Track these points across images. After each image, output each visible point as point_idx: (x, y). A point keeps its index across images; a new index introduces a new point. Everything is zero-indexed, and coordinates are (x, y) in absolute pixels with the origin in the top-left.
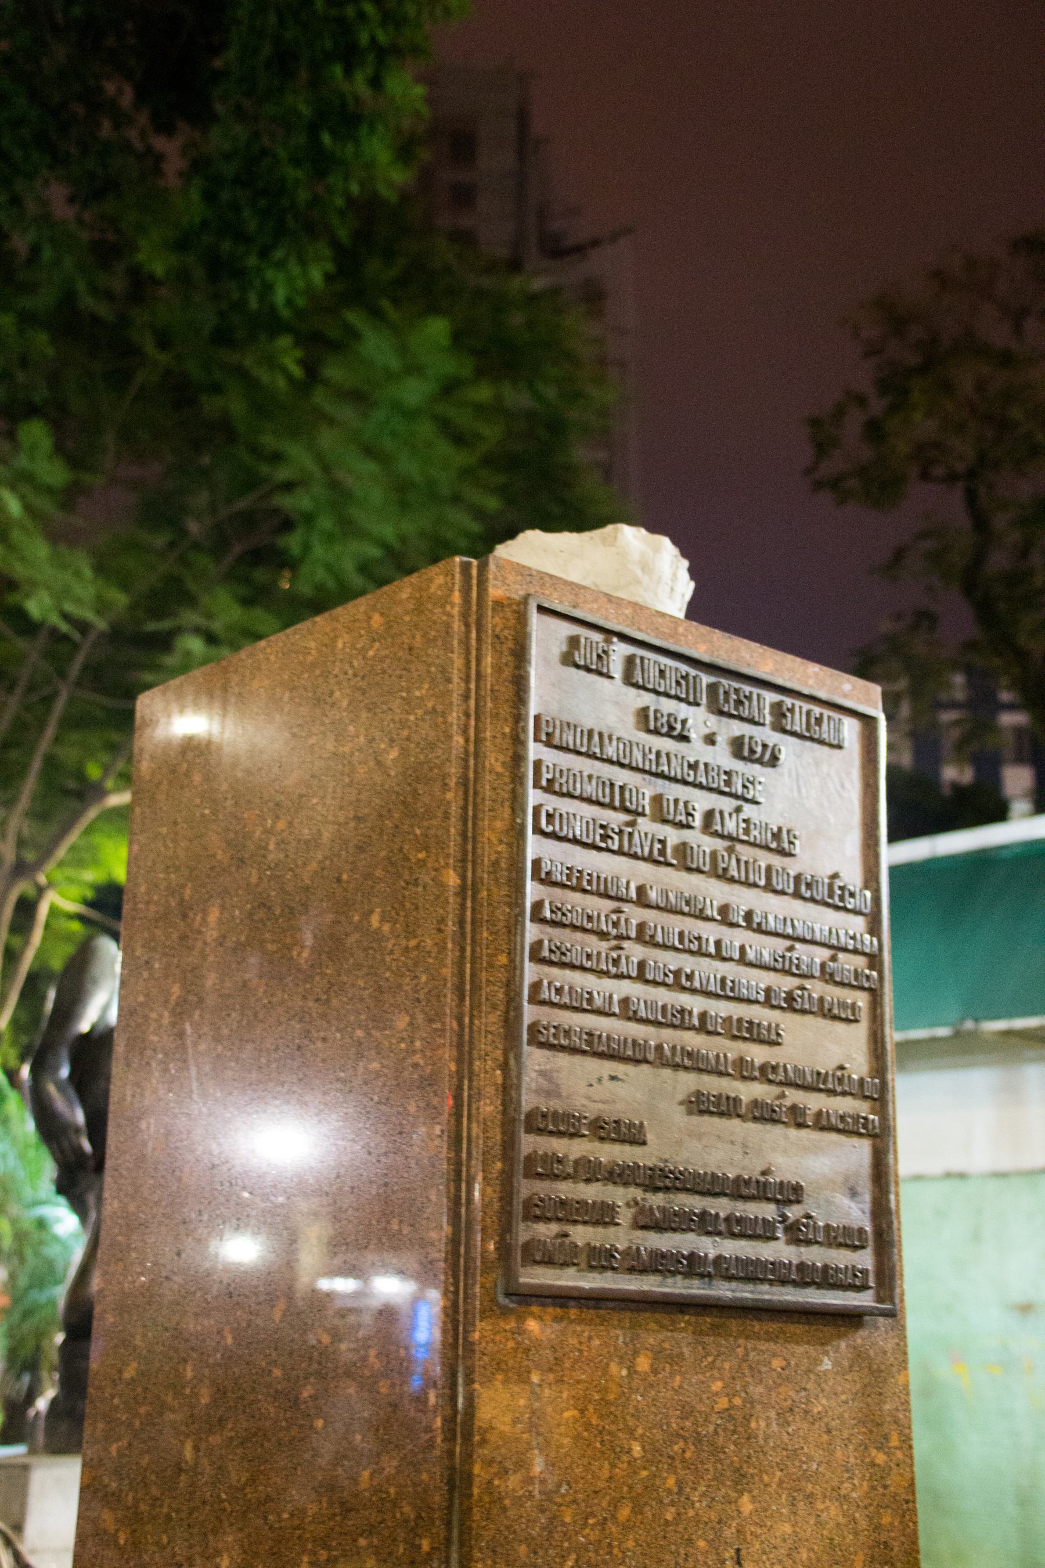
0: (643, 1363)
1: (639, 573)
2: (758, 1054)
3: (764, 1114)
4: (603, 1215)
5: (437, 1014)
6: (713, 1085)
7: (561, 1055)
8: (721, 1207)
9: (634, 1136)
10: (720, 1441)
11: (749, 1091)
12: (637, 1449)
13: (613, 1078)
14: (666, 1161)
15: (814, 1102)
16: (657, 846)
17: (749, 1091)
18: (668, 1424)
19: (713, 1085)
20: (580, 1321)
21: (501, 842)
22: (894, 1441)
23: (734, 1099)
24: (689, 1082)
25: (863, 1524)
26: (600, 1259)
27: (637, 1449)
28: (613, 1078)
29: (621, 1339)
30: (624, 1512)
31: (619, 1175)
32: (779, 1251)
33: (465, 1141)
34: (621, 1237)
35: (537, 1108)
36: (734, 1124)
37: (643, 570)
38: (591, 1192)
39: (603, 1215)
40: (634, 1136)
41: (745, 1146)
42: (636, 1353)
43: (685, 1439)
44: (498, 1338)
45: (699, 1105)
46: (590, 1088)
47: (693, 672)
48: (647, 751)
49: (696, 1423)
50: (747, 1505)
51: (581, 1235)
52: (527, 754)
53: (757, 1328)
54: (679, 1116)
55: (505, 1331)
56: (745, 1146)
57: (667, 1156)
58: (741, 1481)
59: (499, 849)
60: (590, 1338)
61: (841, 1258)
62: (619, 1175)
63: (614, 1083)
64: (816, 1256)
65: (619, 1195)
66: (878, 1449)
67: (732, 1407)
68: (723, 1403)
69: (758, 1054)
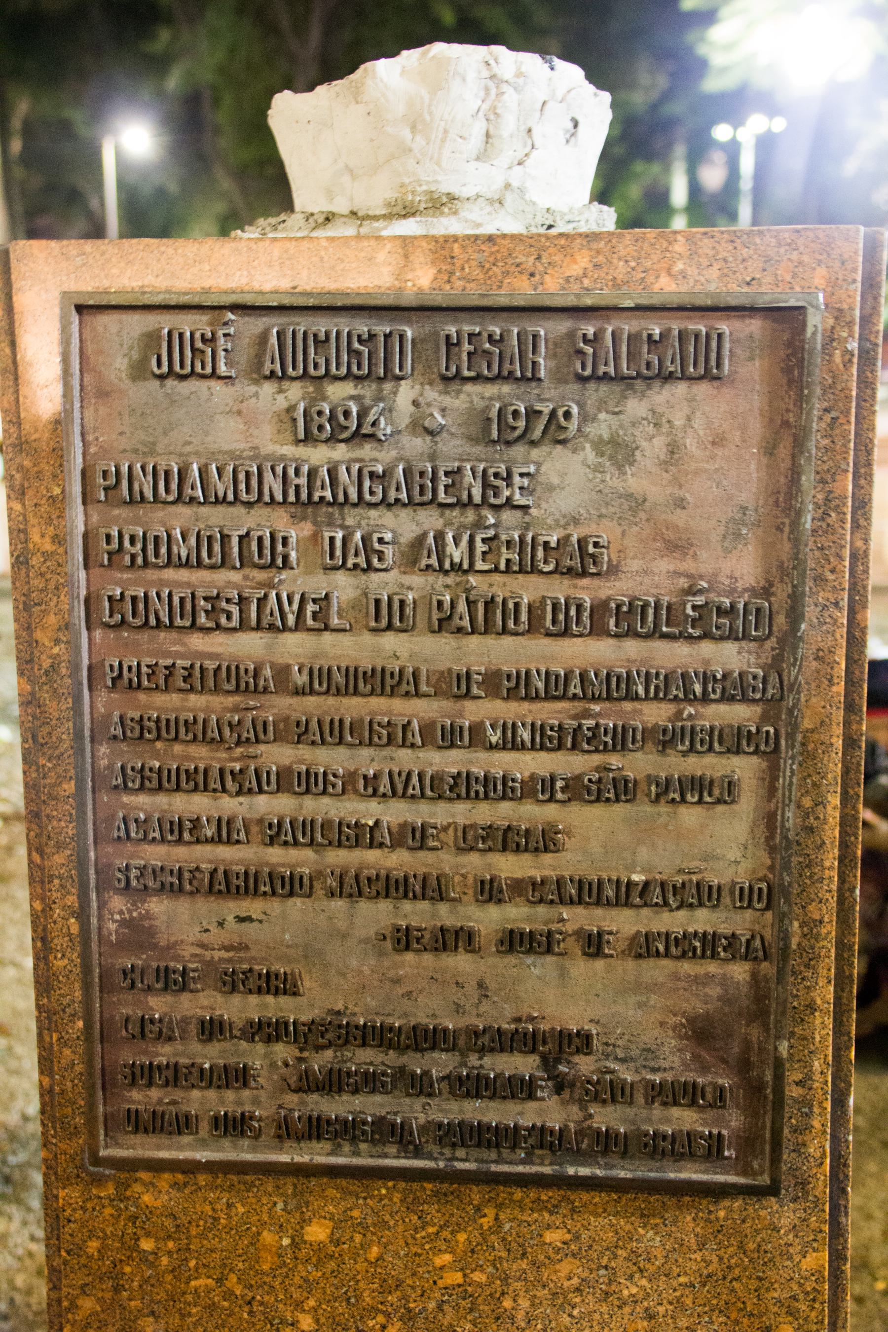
1: (407, 133)
3: (515, 942)
13: (241, 920)
14: (338, 1013)
18: (358, 1298)
19: (416, 913)
20: (213, 1188)
21: (57, 642)
28: (241, 920)
29: (280, 1206)
31: (268, 1031)
32: (550, 1112)
35: (657, 724)
37: (413, 128)
43: (388, 1315)
44: (89, 1205)
46: (205, 935)
47: (382, 329)
48: (291, 472)
49: (405, 1298)
55: (100, 1198)
57: (339, 1006)
59: (56, 650)
60: (229, 1206)
62: (268, 1031)
63: (245, 926)
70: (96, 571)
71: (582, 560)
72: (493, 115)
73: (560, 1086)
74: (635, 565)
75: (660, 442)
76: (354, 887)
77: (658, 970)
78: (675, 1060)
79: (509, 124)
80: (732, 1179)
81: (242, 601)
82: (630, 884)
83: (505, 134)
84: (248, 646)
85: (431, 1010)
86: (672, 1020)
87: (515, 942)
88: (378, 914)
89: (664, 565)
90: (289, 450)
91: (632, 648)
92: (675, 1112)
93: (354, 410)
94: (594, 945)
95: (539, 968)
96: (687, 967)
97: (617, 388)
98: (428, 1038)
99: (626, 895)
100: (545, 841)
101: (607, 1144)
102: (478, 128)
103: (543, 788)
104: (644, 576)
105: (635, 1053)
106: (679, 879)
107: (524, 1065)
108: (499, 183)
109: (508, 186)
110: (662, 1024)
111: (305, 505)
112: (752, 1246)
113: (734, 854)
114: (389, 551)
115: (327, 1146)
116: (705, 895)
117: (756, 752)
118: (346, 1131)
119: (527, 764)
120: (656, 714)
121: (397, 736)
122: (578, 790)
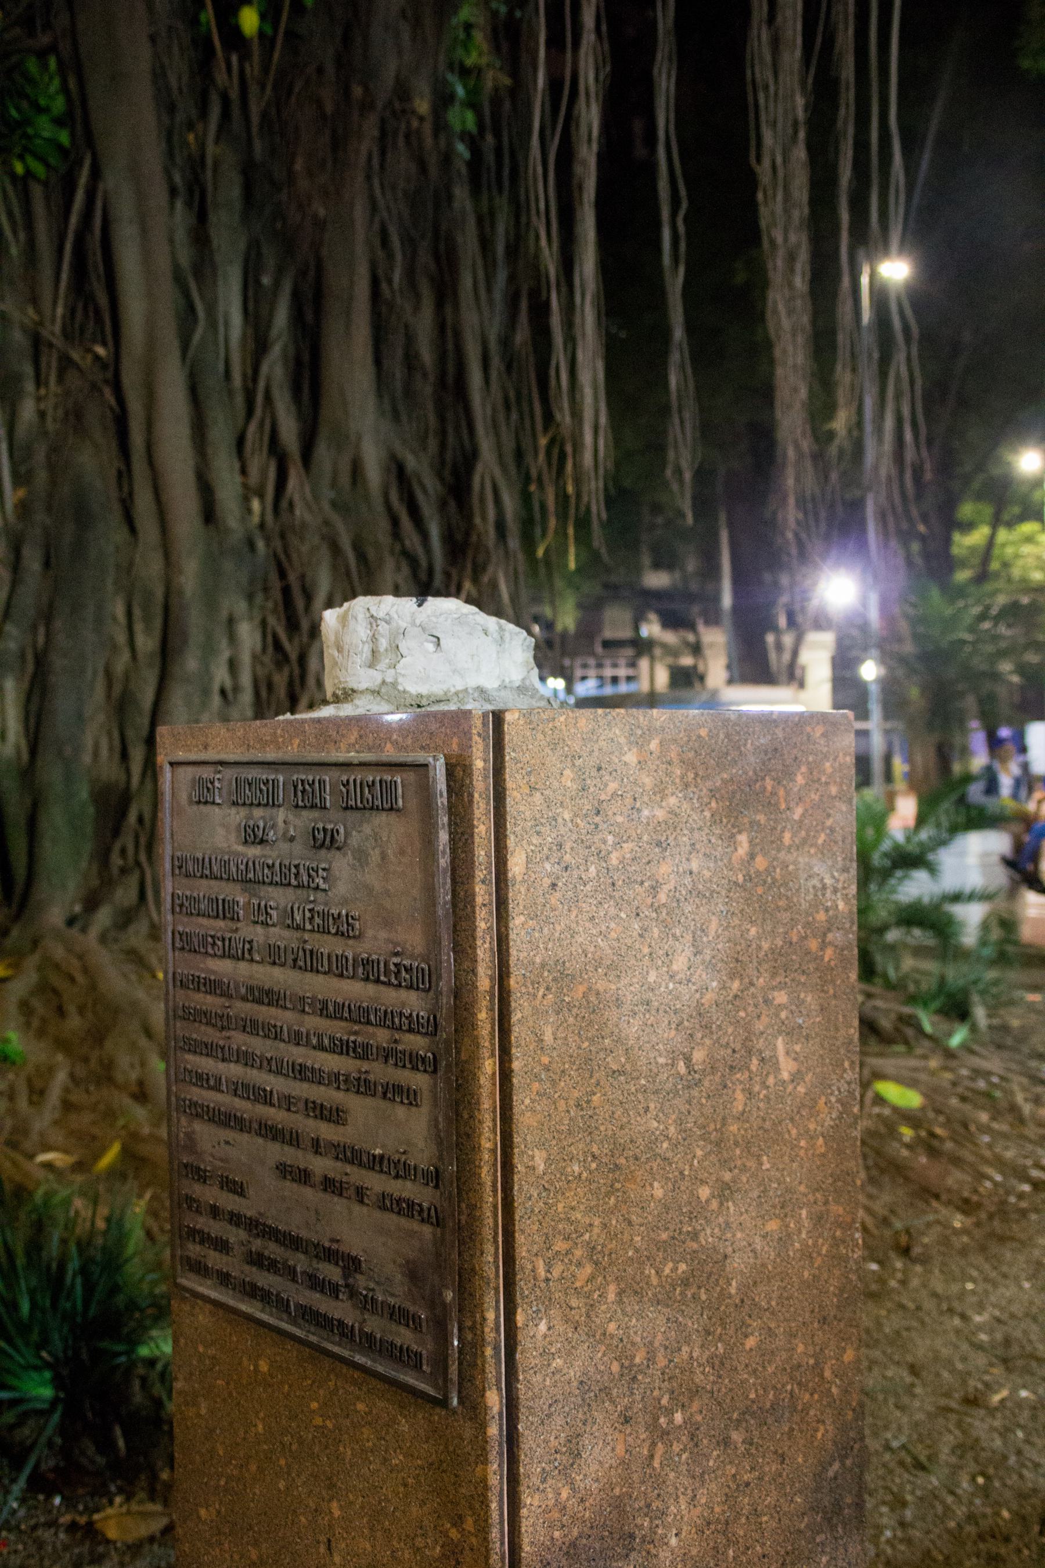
2: (326, 1131)
3: (330, 1185)
4: (222, 1246)
5: (838, 1246)
6: (291, 1155)
8: (300, 1262)
9: (237, 1189)
10: (316, 1449)
11: (321, 1165)
13: (227, 1143)
15: (376, 1183)
16: (247, 946)
17: (321, 1165)
22: (469, 1524)
23: (305, 1171)
28: (227, 1143)
34: (232, 1264)
36: (308, 1192)
38: (216, 1228)
39: (222, 1246)
40: (237, 1189)
41: (317, 1212)
42: (259, 1356)
45: (284, 1170)
52: (797, 714)
53: (344, 1371)
54: (270, 1180)
56: (317, 1212)
63: (227, 1147)
65: (235, 1235)
66: (454, 1525)
67: (324, 1427)
69: (326, 1131)
70: (177, 916)
71: (345, 928)
72: (374, 639)
73: (353, 1293)
74: (370, 933)
75: (377, 851)
76: (271, 1132)
77: (392, 1220)
78: (399, 1290)
79: (383, 644)
80: (422, 1386)
81: (223, 940)
82: (374, 1156)
83: (382, 649)
84: (222, 968)
85: (294, 1224)
86: (400, 1260)
87: (330, 1185)
88: (276, 1152)
89: (383, 935)
90: (240, 848)
91: (371, 989)
92: (402, 1330)
93: (261, 825)
94: (360, 1194)
95: (339, 1205)
96: (403, 1221)
97: (357, 815)
98: (294, 1243)
99: (376, 1163)
100: (334, 1115)
101: (369, 1343)
102: (367, 649)
103: (336, 1080)
104: (374, 942)
105: (383, 1279)
106: (396, 1157)
107: (332, 1272)
108: (379, 681)
109: (384, 682)
110: (394, 1262)
111: (248, 882)
112: (451, 1449)
113: (421, 1144)
114: (274, 913)
115: (259, 1305)
116: (402, 1170)
117: (425, 1071)
118: (263, 1296)
119: (331, 1062)
120: (381, 1036)
121: (274, 1033)
122: (363, 1086)
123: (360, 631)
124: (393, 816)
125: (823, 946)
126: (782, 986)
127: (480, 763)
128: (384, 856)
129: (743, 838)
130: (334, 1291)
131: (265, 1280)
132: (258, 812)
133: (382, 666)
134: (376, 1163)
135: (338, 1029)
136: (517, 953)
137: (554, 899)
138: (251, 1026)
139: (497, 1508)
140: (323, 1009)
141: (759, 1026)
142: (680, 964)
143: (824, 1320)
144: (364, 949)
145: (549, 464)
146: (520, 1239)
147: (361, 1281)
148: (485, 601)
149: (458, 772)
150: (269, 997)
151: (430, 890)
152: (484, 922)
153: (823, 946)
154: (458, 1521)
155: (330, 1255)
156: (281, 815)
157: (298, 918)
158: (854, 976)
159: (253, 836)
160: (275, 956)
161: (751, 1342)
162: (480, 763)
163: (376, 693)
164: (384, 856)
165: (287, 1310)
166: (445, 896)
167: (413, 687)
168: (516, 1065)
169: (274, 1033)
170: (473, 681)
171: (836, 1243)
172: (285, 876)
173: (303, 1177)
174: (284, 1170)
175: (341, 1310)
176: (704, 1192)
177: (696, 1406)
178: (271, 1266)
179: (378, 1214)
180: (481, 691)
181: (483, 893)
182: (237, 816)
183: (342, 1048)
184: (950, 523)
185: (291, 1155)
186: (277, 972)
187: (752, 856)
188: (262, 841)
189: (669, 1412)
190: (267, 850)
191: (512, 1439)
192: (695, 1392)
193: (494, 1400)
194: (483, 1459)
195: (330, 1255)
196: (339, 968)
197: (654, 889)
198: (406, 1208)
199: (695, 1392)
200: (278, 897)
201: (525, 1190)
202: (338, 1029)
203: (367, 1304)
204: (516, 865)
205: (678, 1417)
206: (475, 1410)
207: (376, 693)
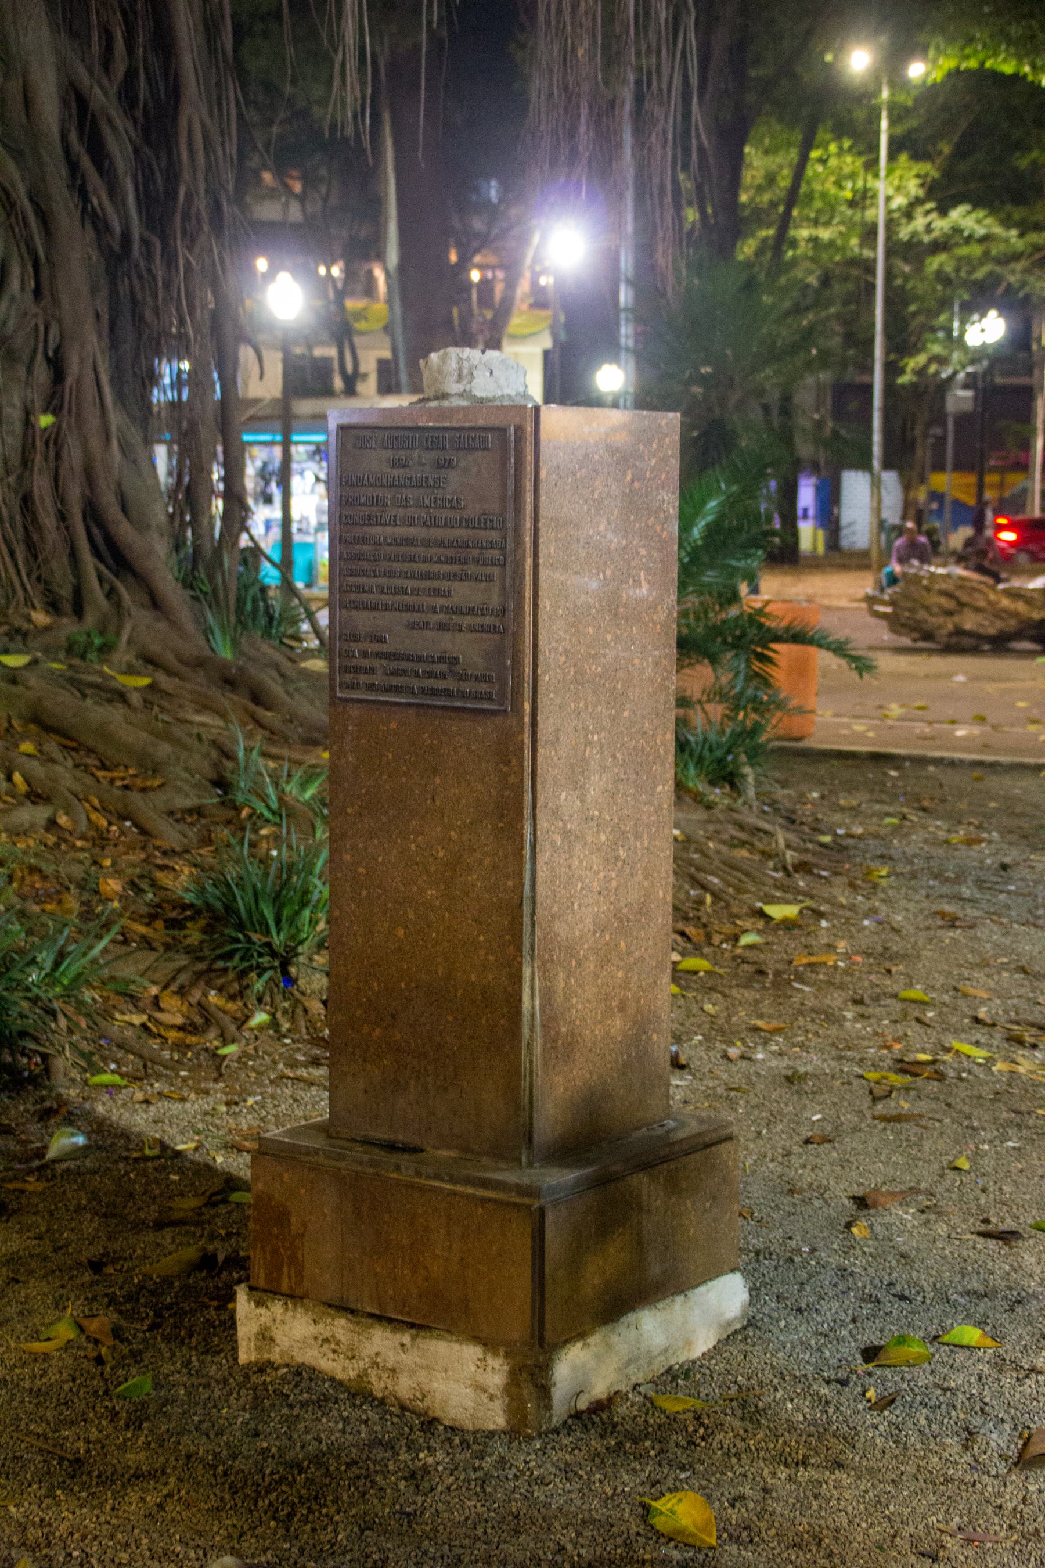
0: (393, 726)
2: (440, 602)
3: (442, 627)
4: (372, 671)
6: (416, 617)
7: (845, 520)
12: (390, 756)
15: (467, 620)
22: (514, 762)
24: (407, 616)
25: (494, 793)
26: (370, 687)
27: (390, 756)
30: (385, 777)
31: (378, 655)
33: (786, 744)
34: (378, 679)
36: (428, 633)
40: (382, 640)
45: (412, 626)
50: (438, 781)
51: (363, 679)
58: (435, 771)
61: (484, 687)
62: (378, 655)
64: (467, 687)
65: (376, 663)
68: (428, 742)
79: (465, 371)
91: (470, 532)
95: (447, 636)
99: (471, 611)
103: (447, 577)
104: (472, 509)
107: (443, 667)
123: (453, 365)
124: (485, 453)
125: (663, 530)
126: (643, 546)
127: (529, 429)
128: (479, 471)
129: (629, 473)
130: (444, 677)
131: (397, 681)
132: (402, 453)
133: (465, 382)
134: (471, 611)
135: (450, 552)
136: (543, 512)
137: (556, 490)
138: (397, 559)
139: (527, 753)
140: (440, 544)
141: (633, 564)
142: (602, 528)
143: (657, 715)
144: (465, 514)
145: (211, 116)
146: (540, 637)
147: (458, 668)
148: (619, 366)
149: (519, 429)
150: (409, 542)
151: (504, 486)
152: (529, 498)
153: (663, 530)
154: (508, 763)
155: (441, 660)
156: (416, 454)
157: (427, 502)
158: (676, 548)
159: (397, 464)
160: (409, 522)
161: (626, 714)
162: (529, 429)
163: (460, 395)
164: (479, 471)
165: (413, 693)
166: (511, 487)
167: (479, 393)
168: (541, 561)
169: (411, 559)
170: (507, 391)
171: (664, 679)
172: (420, 483)
173: (426, 625)
174: (412, 626)
175: (450, 684)
176: (609, 637)
177: (603, 734)
178: (404, 673)
179: (469, 634)
180: (509, 396)
181: (529, 485)
182: (386, 454)
183: (452, 561)
184: (732, 138)
185: (416, 617)
186: (412, 529)
187: (633, 481)
188: (404, 466)
189: (593, 734)
190: (407, 470)
191: (534, 724)
192: (603, 728)
193: (527, 707)
194: (522, 731)
195: (441, 660)
196: (449, 524)
197: (593, 491)
198: (483, 629)
199: (603, 728)
200: (411, 494)
201: (542, 616)
202: (450, 552)
203: (462, 678)
204: (543, 474)
205: (596, 737)
206: (518, 711)
207: (460, 395)
